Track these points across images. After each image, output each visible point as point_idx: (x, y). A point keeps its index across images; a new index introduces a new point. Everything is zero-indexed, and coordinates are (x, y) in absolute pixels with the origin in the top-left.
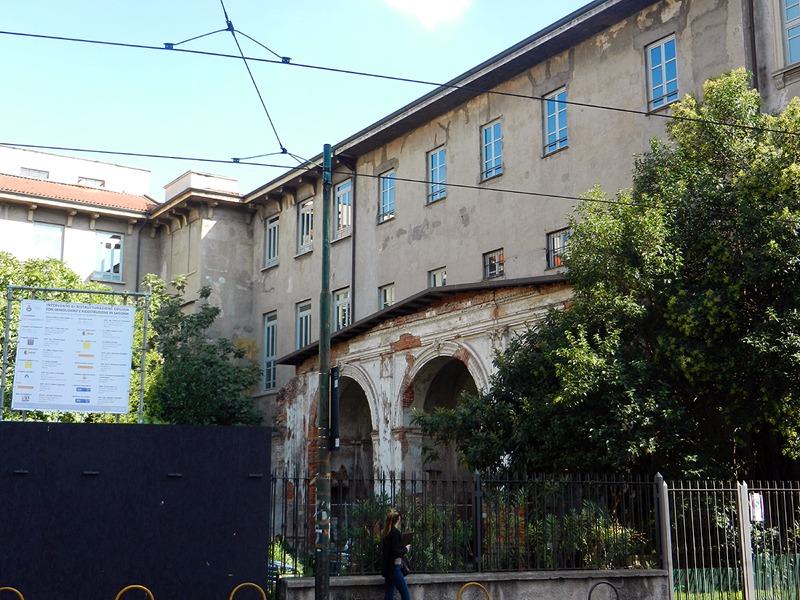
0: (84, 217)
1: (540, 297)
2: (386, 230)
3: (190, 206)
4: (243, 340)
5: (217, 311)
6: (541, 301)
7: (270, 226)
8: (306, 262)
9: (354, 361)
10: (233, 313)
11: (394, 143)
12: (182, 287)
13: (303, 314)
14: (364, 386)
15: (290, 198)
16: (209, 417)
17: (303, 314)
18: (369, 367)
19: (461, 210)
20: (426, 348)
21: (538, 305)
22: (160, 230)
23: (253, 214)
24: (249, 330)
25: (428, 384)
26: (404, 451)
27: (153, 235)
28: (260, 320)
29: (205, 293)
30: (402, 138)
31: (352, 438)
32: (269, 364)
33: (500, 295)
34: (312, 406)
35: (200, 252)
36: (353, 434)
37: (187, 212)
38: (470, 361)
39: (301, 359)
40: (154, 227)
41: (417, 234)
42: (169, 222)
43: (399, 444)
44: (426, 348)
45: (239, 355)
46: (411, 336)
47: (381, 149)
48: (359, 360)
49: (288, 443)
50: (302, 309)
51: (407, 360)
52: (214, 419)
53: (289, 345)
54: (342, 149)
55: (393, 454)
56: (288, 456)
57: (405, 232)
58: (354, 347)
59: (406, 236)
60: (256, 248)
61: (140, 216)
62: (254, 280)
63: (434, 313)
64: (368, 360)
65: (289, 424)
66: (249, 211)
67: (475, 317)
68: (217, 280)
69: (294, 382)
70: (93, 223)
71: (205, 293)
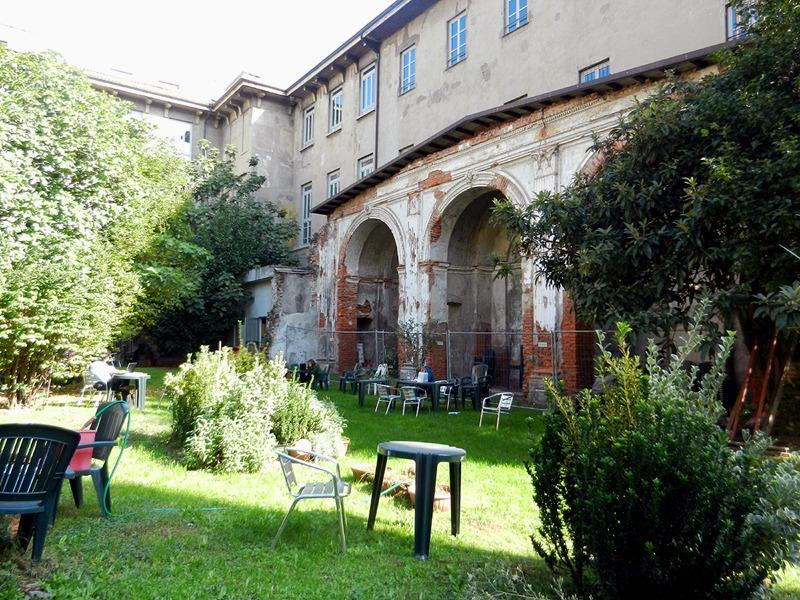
0: (158, 105)
1: (605, 105)
2: (409, 99)
3: (244, 96)
4: (285, 205)
5: (263, 179)
6: (605, 109)
7: (307, 115)
8: (336, 139)
9: (382, 203)
10: (278, 185)
11: (416, 21)
12: (233, 154)
13: (332, 182)
14: (391, 225)
15: (324, 89)
16: (253, 258)
17: (332, 182)
18: (395, 207)
19: (482, 67)
20: (456, 182)
21: (605, 114)
22: (222, 122)
23: (294, 106)
24: (290, 199)
25: (455, 220)
26: (431, 283)
27: (216, 126)
28: (299, 191)
29: (253, 163)
30: (423, 15)
31: (376, 277)
32: (305, 225)
33: (551, 111)
34: (342, 247)
35: (251, 135)
36: (376, 273)
37: (241, 104)
38: (509, 188)
39: (329, 208)
40: (216, 118)
41: (437, 97)
42: (229, 115)
43: (426, 277)
44: (456, 182)
45: (282, 215)
46: (440, 173)
47: (403, 29)
48: (386, 202)
49: (320, 280)
50: (332, 178)
51: (436, 196)
52: (258, 261)
53: (321, 195)
54: (369, 31)
55: (420, 285)
56: (320, 291)
57: (424, 98)
58: (382, 191)
59: (426, 101)
60: (296, 134)
61: (205, 109)
62: (294, 159)
63: (468, 144)
64: (394, 201)
65: (321, 264)
66: (290, 103)
67: (516, 142)
68: (265, 158)
69: (326, 228)
70: (167, 112)
71: (253, 163)
